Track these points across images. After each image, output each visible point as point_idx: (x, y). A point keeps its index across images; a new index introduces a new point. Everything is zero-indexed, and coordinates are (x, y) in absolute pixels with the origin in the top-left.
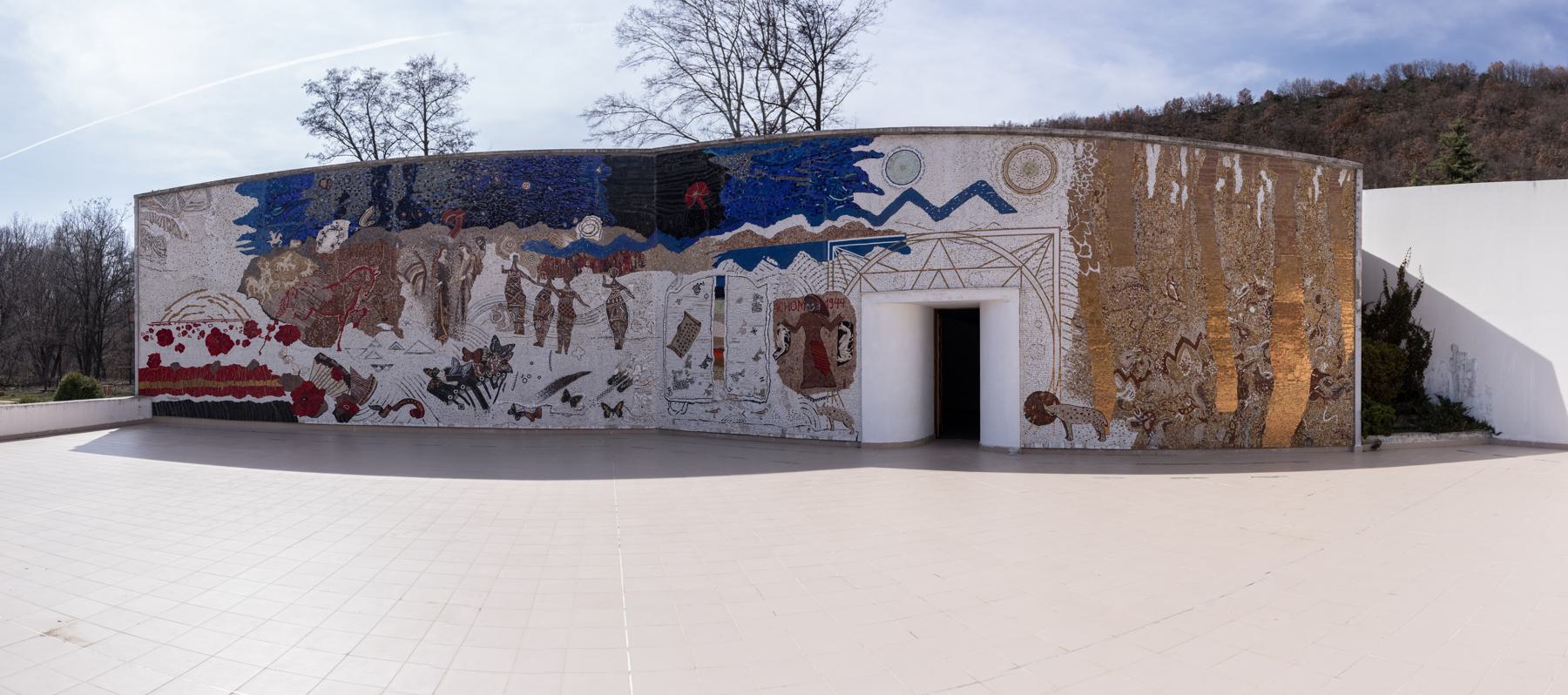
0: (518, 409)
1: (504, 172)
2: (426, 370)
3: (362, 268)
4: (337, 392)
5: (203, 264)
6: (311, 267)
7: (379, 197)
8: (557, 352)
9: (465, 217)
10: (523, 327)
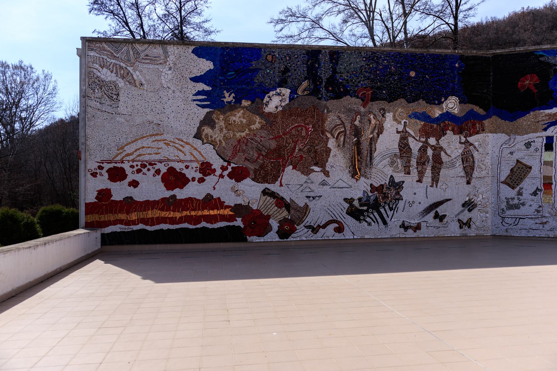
0: (406, 224)
1: (398, 63)
3: (300, 126)
4: (279, 217)
5: (160, 112)
6: (259, 122)
8: (430, 186)
10: (409, 170)
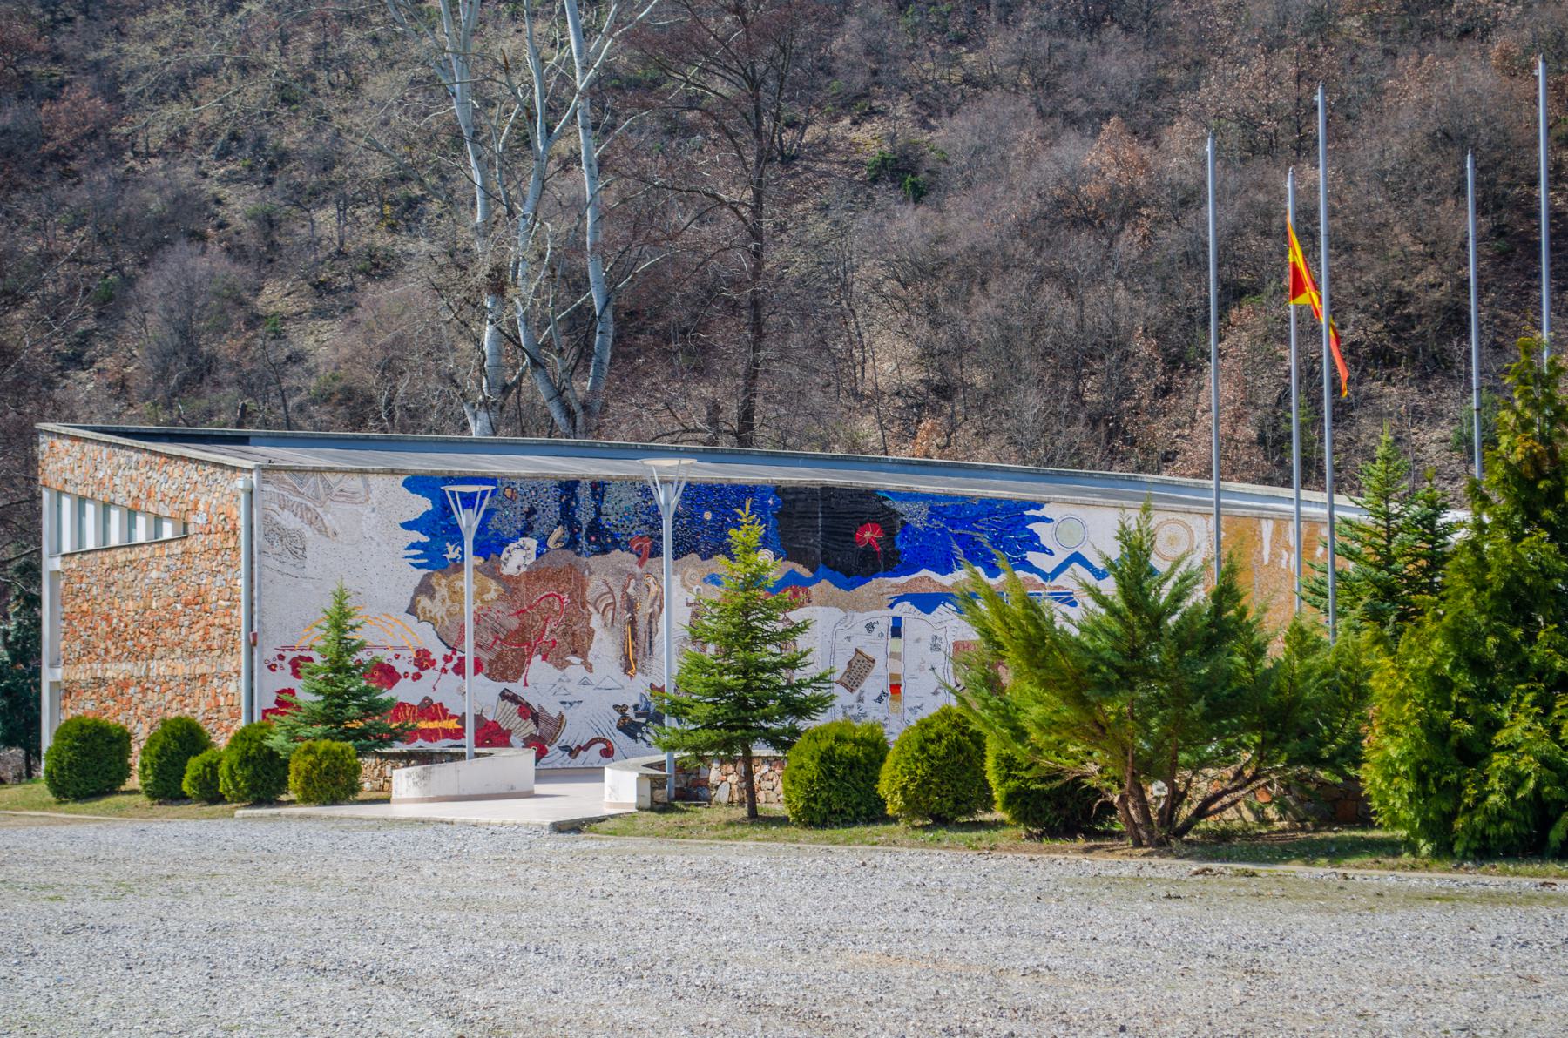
2: (615, 707)
7: (567, 516)
9: (652, 545)
